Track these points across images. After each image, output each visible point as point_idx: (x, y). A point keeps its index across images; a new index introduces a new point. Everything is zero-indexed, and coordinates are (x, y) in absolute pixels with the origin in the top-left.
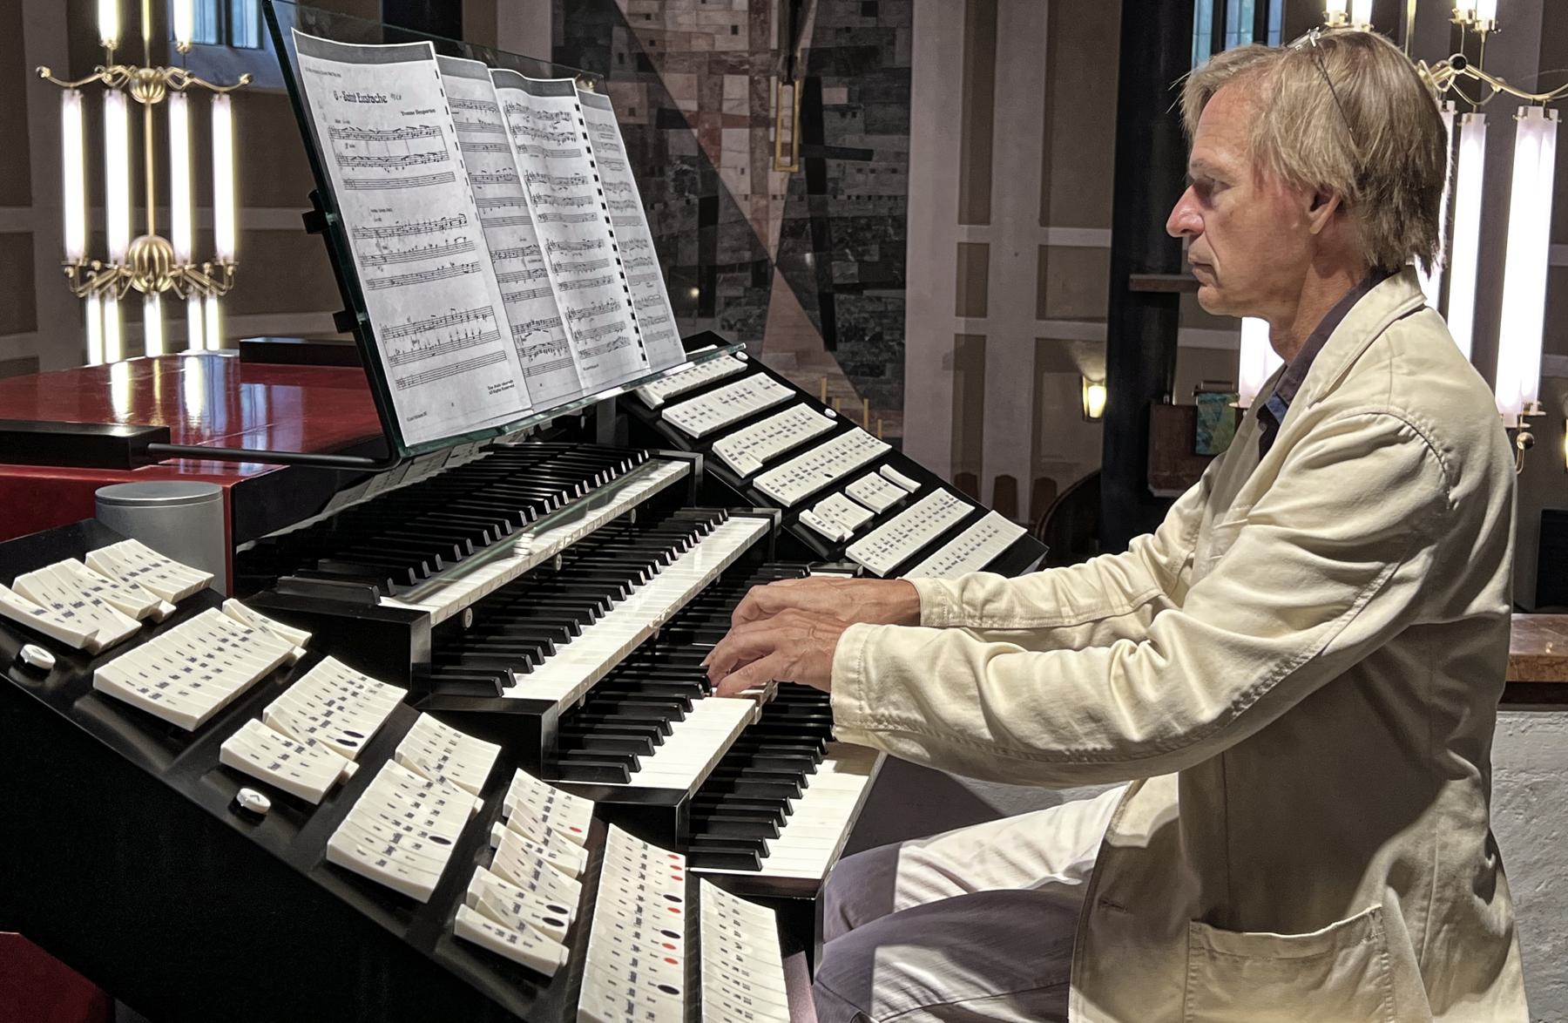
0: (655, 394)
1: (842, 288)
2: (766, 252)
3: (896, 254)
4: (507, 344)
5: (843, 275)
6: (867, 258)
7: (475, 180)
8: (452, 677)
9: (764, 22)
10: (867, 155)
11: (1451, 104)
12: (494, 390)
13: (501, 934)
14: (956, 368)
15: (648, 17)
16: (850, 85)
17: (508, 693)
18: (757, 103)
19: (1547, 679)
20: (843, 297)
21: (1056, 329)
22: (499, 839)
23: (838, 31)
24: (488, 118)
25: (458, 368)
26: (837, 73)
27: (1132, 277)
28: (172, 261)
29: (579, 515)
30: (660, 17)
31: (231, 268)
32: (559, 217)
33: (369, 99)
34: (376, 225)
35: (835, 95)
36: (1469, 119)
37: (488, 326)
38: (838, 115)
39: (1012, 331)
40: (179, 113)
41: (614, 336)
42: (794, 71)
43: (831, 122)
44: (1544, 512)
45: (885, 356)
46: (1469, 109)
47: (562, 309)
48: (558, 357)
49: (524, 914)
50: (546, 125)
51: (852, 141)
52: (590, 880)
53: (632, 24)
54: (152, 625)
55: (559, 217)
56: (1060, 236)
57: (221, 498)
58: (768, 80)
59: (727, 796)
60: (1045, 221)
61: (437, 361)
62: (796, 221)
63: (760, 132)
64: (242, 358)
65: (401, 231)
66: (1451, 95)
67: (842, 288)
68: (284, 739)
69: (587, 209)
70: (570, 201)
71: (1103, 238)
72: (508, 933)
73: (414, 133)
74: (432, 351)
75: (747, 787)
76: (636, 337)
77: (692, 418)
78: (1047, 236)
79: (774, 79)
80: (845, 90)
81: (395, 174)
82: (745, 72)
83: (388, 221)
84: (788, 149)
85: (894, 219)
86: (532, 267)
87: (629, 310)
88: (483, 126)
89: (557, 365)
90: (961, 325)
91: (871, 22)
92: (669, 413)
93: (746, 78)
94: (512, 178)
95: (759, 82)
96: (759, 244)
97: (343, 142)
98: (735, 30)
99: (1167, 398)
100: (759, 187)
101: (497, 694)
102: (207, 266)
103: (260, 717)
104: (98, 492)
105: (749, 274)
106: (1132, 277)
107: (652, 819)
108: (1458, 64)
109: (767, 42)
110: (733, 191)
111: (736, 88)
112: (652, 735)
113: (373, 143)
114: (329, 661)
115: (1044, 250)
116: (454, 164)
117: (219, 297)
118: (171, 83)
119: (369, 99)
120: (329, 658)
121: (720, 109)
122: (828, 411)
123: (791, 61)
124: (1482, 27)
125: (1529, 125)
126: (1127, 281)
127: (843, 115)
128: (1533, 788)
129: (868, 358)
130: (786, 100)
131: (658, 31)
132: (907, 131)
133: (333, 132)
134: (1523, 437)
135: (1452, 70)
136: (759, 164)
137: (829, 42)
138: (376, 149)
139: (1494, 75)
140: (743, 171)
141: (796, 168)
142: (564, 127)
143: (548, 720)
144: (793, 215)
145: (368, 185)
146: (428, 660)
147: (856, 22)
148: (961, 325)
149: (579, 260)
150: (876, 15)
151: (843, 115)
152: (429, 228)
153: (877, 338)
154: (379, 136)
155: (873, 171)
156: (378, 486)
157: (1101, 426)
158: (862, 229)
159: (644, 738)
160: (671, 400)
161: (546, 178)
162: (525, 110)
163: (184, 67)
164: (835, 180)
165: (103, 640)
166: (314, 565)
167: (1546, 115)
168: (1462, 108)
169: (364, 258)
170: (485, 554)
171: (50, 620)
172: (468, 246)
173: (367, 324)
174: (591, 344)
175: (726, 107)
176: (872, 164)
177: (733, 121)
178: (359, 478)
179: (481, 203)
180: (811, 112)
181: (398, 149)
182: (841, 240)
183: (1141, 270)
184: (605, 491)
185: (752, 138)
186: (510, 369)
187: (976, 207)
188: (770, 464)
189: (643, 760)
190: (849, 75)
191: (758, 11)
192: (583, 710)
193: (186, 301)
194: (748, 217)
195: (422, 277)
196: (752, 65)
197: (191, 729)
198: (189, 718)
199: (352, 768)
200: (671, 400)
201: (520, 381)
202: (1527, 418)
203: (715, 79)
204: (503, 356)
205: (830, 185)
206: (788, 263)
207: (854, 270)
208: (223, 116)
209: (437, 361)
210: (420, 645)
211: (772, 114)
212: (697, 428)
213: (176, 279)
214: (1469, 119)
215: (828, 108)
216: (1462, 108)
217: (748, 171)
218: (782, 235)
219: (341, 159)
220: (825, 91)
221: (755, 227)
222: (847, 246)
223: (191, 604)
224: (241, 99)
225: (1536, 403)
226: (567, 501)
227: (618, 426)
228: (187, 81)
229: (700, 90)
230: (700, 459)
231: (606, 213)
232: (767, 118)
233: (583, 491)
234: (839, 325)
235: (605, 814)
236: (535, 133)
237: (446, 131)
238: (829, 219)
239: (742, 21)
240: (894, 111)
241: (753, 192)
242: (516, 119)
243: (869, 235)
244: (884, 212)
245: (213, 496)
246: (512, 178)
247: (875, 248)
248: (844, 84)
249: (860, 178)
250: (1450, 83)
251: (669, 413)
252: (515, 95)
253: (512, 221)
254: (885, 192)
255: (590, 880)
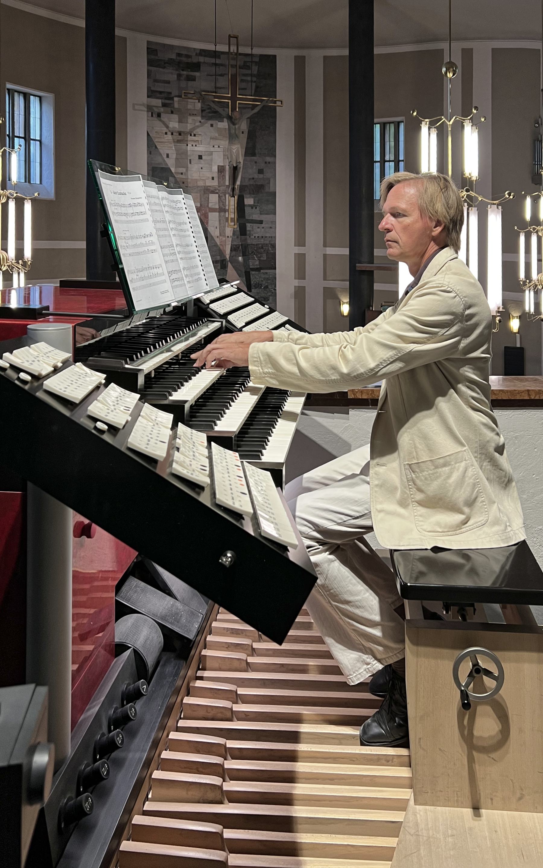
0: (206, 299)
1: (253, 269)
2: (225, 257)
3: (273, 257)
4: (166, 277)
5: (253, 265)
6: (262, 259)
7: (155, 222)
8: (154, 389)
9: (223, 176)
10: (261, 222)
11: (466, 204)
12: (162, 293)
13: (188, 472)
14: (295, 298)
15: (182, 174)
16: (254, 198)
17: (171, 398)
18: (221, 204)
19: (518, 398)
20: (253, 272)
21: (331, 284)
22: (180, 444)
23: (250, 179)
24: (157, 201)
25: (150, 285)
26: (250, 194)
27: (357, 265)
28: (7, 259)
29: (187, 339)
30: (186, 174)
31: (30, 262)
32: (179, 235)
33: (121, 194)
34: (124, 235)
35: (249, 201)
36: (472, 209)
37: (160, 271)
38: (250, 208)
39: (315, 284)
40: (12, 206)
41: (197, 277)
42: (234, 193)
43: (247, 210)
44: (505, 347)
45: (269, 294)
46: (471, 206)
47: (181, 267)
48: (181, 283)
49: (193, 467)
50: (173, 205)
51: (256, 217)
52: (210, 458)
53: (176, 176)
54: (56, 370)
55: (179, 235)
56: (330, 251)
57: (72, 329)
58: (225, 196)
59: (246, 436)
60: (325, 245)
61: (144, 283)
62: (236, 245)
63: (222, 214)
64: (60, 286)
65: (132, 238)
66: (465, 201)
67: (253, 269)
68: (106, 408)
69: (187, 233)
70: (181, 230)
71: (346, 251)
72: (190, 472)
73: (135, 205)
74: (142, 279)
75: (253, 432)
76: (204, 277)
77: (220, 307)
78: (326, 251)
79: (227, 196)
80: (253, 199)
81: (130, 218)
82: (217, 193)
83: (128, 234)
84: (232, 220)
85: (271, 245)
86: (172, 252)
87: (201, 268)
88: (156, 204)
89: (181, 286)
90: (296, 283)
91: (261, 176)
92: (212, 306)
93: (217, 195)
94: (164, 222)
95: (222, 196)
96: (223, 254)
97: (114, 207)
98: (213, 178)
99: (371, 308)
100: (222, 233)
101: (167, 398)
102: (20, 261)
103: (97, 400)
104: (28, 327)
105: (219, 264)
106: (357, 265)
107: (225, 441)
108: (467, 191)
109: (224, 182)
110: (213, 235)
111: (214, 199)
112: (219, 414)
113: (123, 208)
114: (112, 384)
115: (325, 256)
116: (148, 216)
117: (25, 273)
118: (9, 195)
119: (121, 194)
120: (112, 384)
121: (208, 206)
122: (266, 306)
123: (233, 189)
124: (474, 178)
125: (492, 211)
126: (355, 266)
127: (252, 208)
128: (516, 438)
129: (263, 295)
130: (232, 203)
131: (186, 179)
132: (275, 214)
133: (111, 204)
134: (498, 318)
135: (465, 193)
136: (222, 225)
137: (246, 183)
138: (123, 210)
139: (479, 195)
140: (216, 228)
141: (236, 227)
142: (179, 205)
143: (187, 406)
144: (235, 243)
145: (122, 222)
146: (143, 387)
147: (256, 176)
148: (296, 283)
149: (186, 250)
150: (263, 174)
151: (252, 208)
152: (140, 237)
153: (267, 287)
154: (123, 206)
155: (263, 228)
156: (121, 327)
157: (348, 318)
158: (260, 248)
159: (218, 415)
160: (212, 302)
161: (174, 222)
162: (167, 199)
163: (14, 190)
164: (250, 231)
165: (44, 373)
166: (99, 354)
167: (498, 208)
168: (470, 206)
169: (121, 246)
170: (157, 352)
171: (25, 365)
172: (153, 243)
173: (123, 269)
174: (191, 279)
175: (210, 205)
176: (263, 225)
177: (213, 210)
178: (114, 322)
179: (158, 230)
180: (241, 207)
181: (130, 210)
182: (253, 252)
183: (360, 262)
184: (193, 332)
185: (220, 216)
186: (167, 286)
187: (300, 240)
188: (248, 324)
189: (218, 422)
190: (254, 194)
191: (221, 172)
192: (194, 406)
193: (12, 274)
194: (219, 244)
195: (138, 254)
196: (219, 190)
197: (77, 402)
198: (77, 399)
199: (129, 419)
200: (212, 302)
201: (170, 290)
202: (499, 312)
203: (206, 195)
204: (165, 281)
205: (248, 232)
206: (233, 260)
207: (257, 263)
208: (28, 207)
209: (144, 283)
210: (141, 380)
211: (227, 208)
212: (222, 311)
213: (9, 266)
214: (472, 209)
215: (246, 205)
216: (470, 206)
217: (218, 228)
218: (231, 250)
219: (113, 213)
220: (245, 200)
221: (221, 247)
222: (255, 254)
223: (66, 364)
224: (34, 201)
225: (501, 307)
226: (182, 335)
227: (194, 310)
228: (15, 195)
229: (201, 199)
230: (224, 321)
231: (193, 235)
232: (225, 209)
233: (163, 344)
234: (252, 282)
235: (210, 439)
236: (171, 207)
237: (146, 204)
238: (248, 245)
239: (216, 175)
240: (271, 207)
241: (220, 235)
242: (165, 202)
243: (262, 250)
244: (268, 242)
245: (69, 328)
246: (164, 222)
247: (264, 255)
248: (252, 197)
249: (259, 230)
250: (465, 197)
251: (212, 306)
252: (164, 194)
253: (165, 236)
254: (268, 235)
255: (210, 458)
